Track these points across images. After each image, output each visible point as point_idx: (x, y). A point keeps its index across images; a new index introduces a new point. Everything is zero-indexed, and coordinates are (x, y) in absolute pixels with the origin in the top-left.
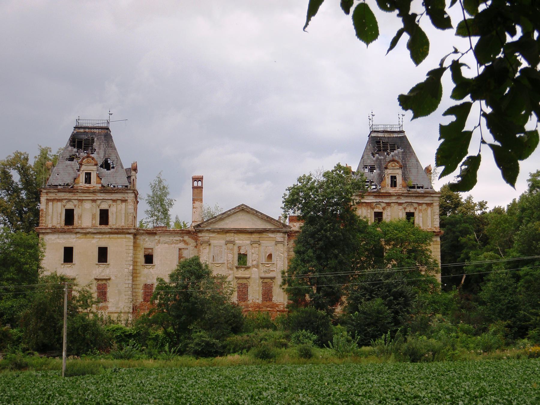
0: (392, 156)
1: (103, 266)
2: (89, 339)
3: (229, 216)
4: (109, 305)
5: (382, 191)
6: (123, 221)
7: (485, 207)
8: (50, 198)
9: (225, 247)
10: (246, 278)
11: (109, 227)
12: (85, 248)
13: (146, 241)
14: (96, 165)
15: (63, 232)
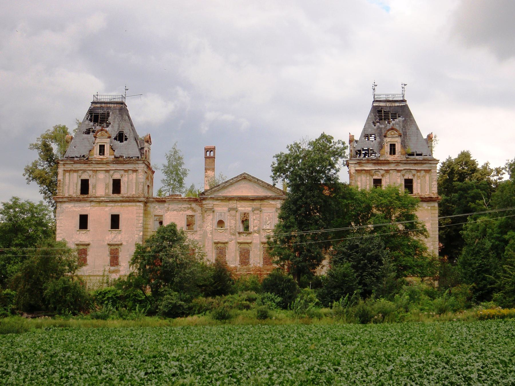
0: (393, 125)
1: (115, 231)
2: (72, 301)
3: (232, 184)
4: (121, 268)
5: (381, 159)
6: (134, 190)
7: (501, 173)
8: (67, 169)
9: (228, 214)
10: (248, 243)
11: (120, 195)
12: (99, 215)
13: (157, 209)
14: (109, 137)
15: (79, 200)
